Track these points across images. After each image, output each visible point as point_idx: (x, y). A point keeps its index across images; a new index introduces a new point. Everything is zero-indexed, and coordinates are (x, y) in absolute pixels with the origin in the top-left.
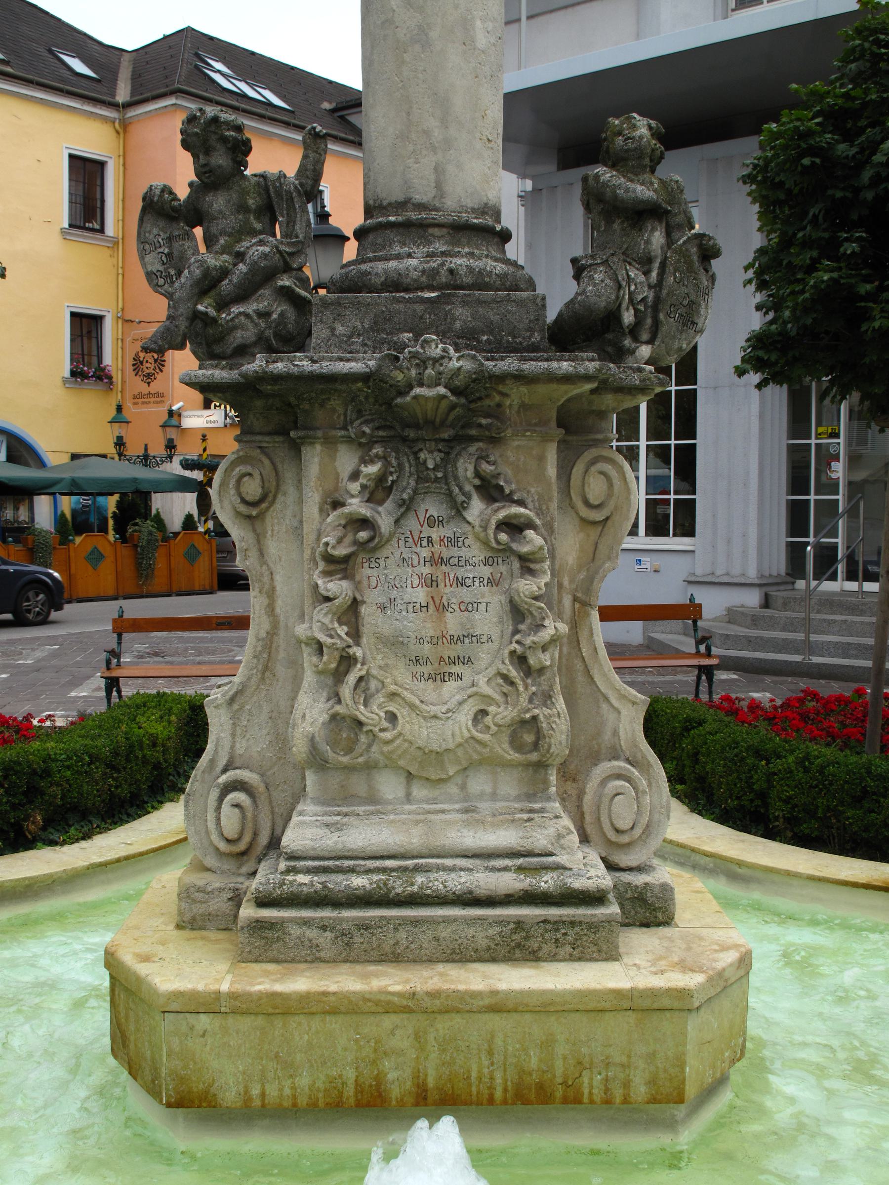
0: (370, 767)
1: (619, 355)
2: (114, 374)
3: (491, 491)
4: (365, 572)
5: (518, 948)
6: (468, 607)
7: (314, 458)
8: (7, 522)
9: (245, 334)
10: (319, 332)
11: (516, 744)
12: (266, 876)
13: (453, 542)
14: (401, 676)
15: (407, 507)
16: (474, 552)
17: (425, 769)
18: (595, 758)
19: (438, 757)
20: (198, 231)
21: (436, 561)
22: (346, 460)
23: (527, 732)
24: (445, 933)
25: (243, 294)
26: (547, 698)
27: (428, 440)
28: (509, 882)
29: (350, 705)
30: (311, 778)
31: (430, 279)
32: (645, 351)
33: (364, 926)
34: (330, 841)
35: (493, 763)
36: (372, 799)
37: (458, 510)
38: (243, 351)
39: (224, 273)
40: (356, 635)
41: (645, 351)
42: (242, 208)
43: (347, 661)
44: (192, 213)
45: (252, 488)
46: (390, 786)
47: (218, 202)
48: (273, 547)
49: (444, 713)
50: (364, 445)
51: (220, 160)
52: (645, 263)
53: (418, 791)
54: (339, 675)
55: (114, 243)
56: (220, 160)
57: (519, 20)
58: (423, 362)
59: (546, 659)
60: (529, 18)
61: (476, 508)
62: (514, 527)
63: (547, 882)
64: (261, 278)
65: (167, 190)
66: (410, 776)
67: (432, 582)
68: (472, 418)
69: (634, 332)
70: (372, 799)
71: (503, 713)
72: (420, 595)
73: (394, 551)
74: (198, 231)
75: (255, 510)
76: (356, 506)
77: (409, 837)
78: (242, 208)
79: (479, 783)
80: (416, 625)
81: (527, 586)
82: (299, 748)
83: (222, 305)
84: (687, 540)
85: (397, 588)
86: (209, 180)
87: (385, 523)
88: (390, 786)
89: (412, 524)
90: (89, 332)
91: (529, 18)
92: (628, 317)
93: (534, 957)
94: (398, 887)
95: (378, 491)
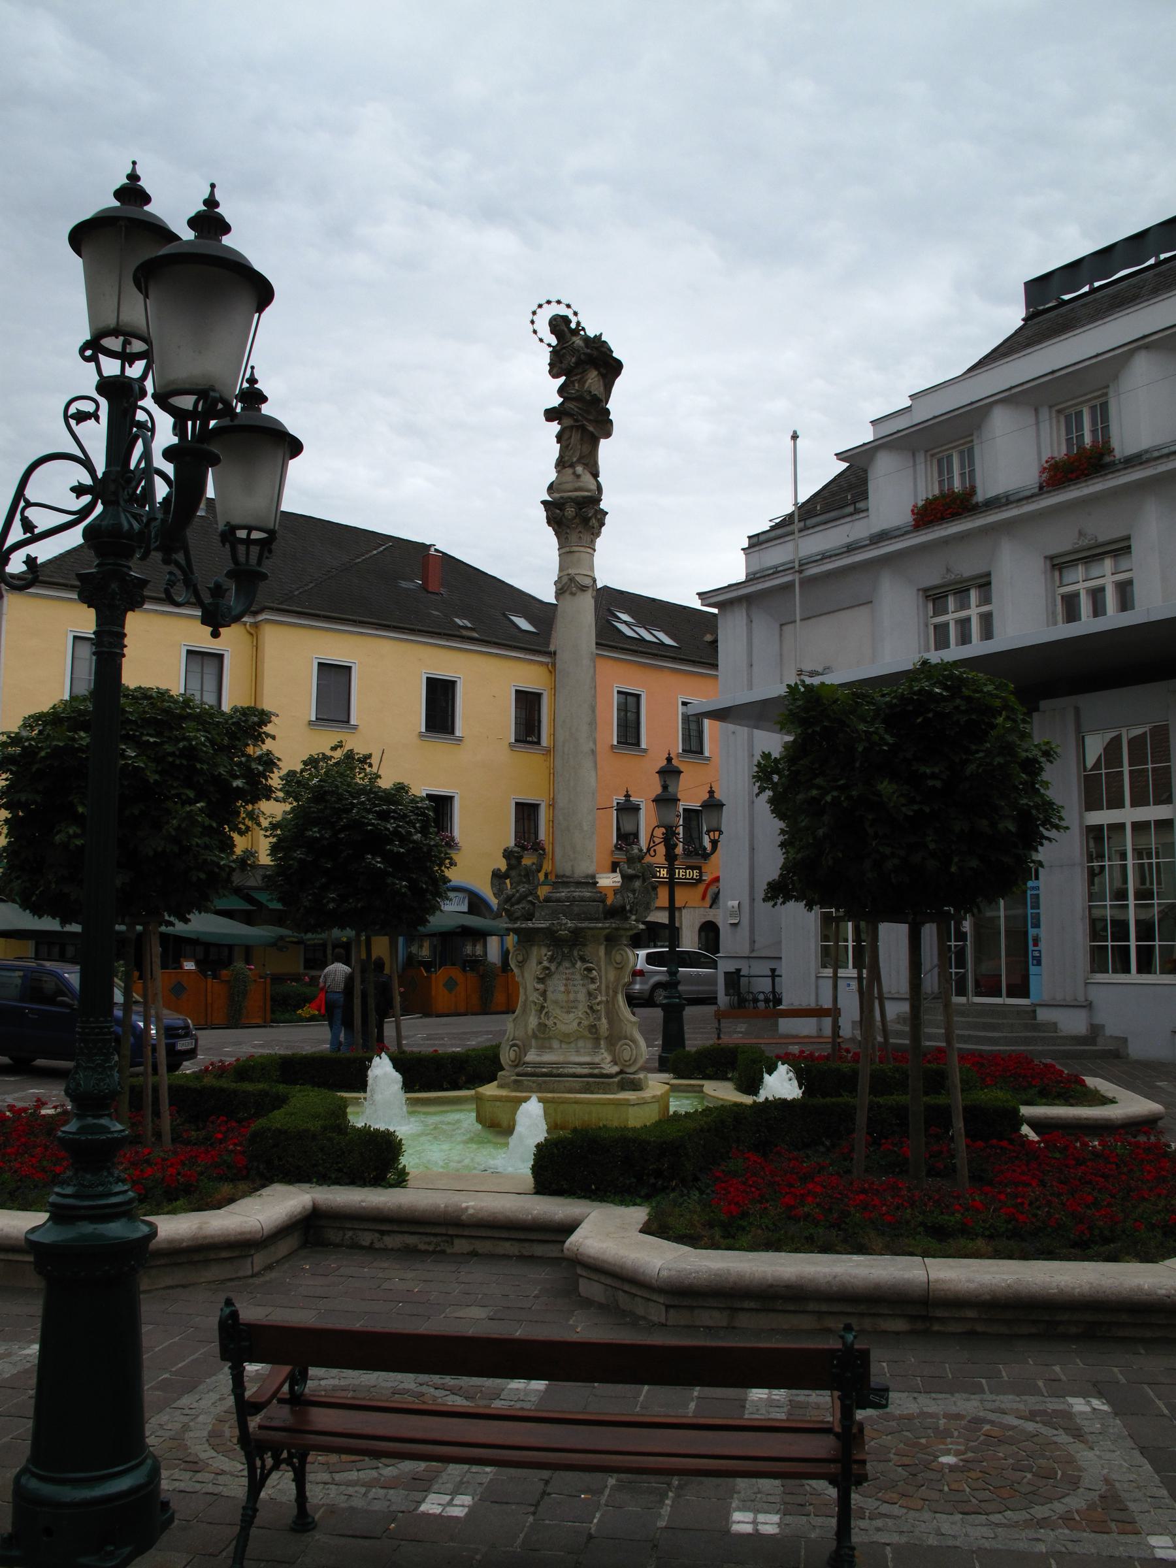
0: (550, 1038)
1: (627, 918)
2: (546, 847)
3: (583, 959)
4: (549, 982)
5: (587, 1089)
6: (576, 992)
7: (535, 950)
8: (467, 955)
9: (518, 914)
10: (537, 914)
11: (591, 1033)
12: (519, 1069)
13: (572, 974)
14: (557, 1012)
15: (559, 964)
16: (578, 977)
17: (565, 1039)
18: (620, 1039)
19: (567, 1035)
20: (508, 881)
21: (567, 979)
22: (544, 950)
23: (593, 1028)
24: (567, 1084)
25: (518, 902)
26: (599, 1019)
27: (566, 946)
28: (586, 1071)
29: (543, 1020)
30: (533, 1041)
31: (568, 899)
32: (633, 917)
33: (545, 1082)
34: (538, 1059)
35: (583, 1037)
36: (550, 1048)
37: (574, 965)
38: (517, 919)
39: (513, 895)
40: (545, 1000)
41: (633, 917)
42: (520, 875)
43: (543, 1007)
44: (506, 876)
45: (520, 958)
46: (556, 1044)
47: (513, 873)
48: (526, 975)
49: (569, 1022)
50: (548, 946)
51: (513, 862)
52: (634, 891)
53: (564, 1046)
54: (541, 1011)
55: (548, 752)
56: (513, 862)
57: (795, 622)
58: (561, 925)
59: (599, 1008)
60: (801, 620)
61: (579, 964)
62: (589, 970)
63: (596, 1071)
64: (523, 898)
65: (499, 870)
66: (561, 1041)
67: (566, 985)
68: (577, 939)
69: (631, 911)
70: (550, 1048)
71: (586, 1023)
72: (562, 989)
73: (556, 976)
74: (508, 881)
75: (521, 964)
76: (545, 963)
77: (561, 1059)
78: (520, 875)
79: (581, 1043)
80: (561, 997)
81: (592, 986)
82: (530, 1032)
83: (512, 905)
84: (1123, 976)
85: (557, 986)
86: (510, 867)
87: (553, 968)
88: (556, 1044)
89: (561, 968)
90: (529, 815)
91: (801, 620)
92: (628, 908)
93: (592, 1093)
94: (555, 1071)
95: (551, 960)
